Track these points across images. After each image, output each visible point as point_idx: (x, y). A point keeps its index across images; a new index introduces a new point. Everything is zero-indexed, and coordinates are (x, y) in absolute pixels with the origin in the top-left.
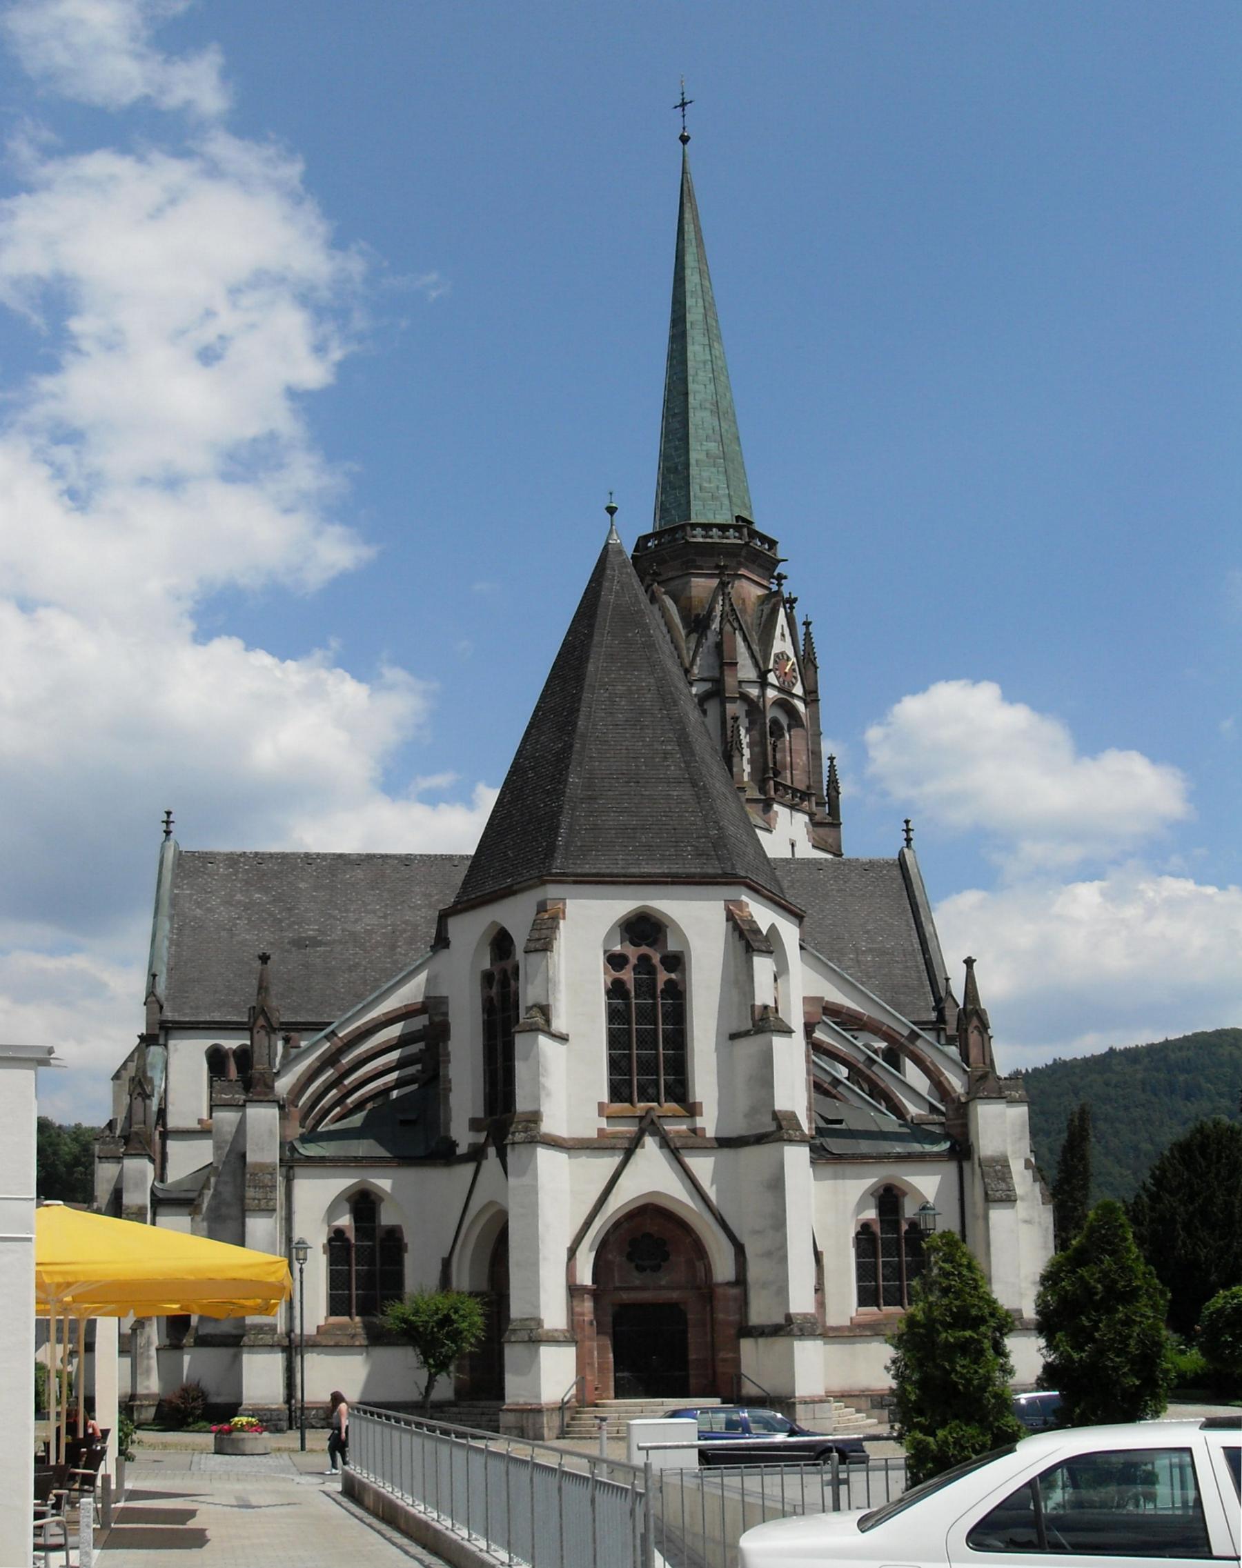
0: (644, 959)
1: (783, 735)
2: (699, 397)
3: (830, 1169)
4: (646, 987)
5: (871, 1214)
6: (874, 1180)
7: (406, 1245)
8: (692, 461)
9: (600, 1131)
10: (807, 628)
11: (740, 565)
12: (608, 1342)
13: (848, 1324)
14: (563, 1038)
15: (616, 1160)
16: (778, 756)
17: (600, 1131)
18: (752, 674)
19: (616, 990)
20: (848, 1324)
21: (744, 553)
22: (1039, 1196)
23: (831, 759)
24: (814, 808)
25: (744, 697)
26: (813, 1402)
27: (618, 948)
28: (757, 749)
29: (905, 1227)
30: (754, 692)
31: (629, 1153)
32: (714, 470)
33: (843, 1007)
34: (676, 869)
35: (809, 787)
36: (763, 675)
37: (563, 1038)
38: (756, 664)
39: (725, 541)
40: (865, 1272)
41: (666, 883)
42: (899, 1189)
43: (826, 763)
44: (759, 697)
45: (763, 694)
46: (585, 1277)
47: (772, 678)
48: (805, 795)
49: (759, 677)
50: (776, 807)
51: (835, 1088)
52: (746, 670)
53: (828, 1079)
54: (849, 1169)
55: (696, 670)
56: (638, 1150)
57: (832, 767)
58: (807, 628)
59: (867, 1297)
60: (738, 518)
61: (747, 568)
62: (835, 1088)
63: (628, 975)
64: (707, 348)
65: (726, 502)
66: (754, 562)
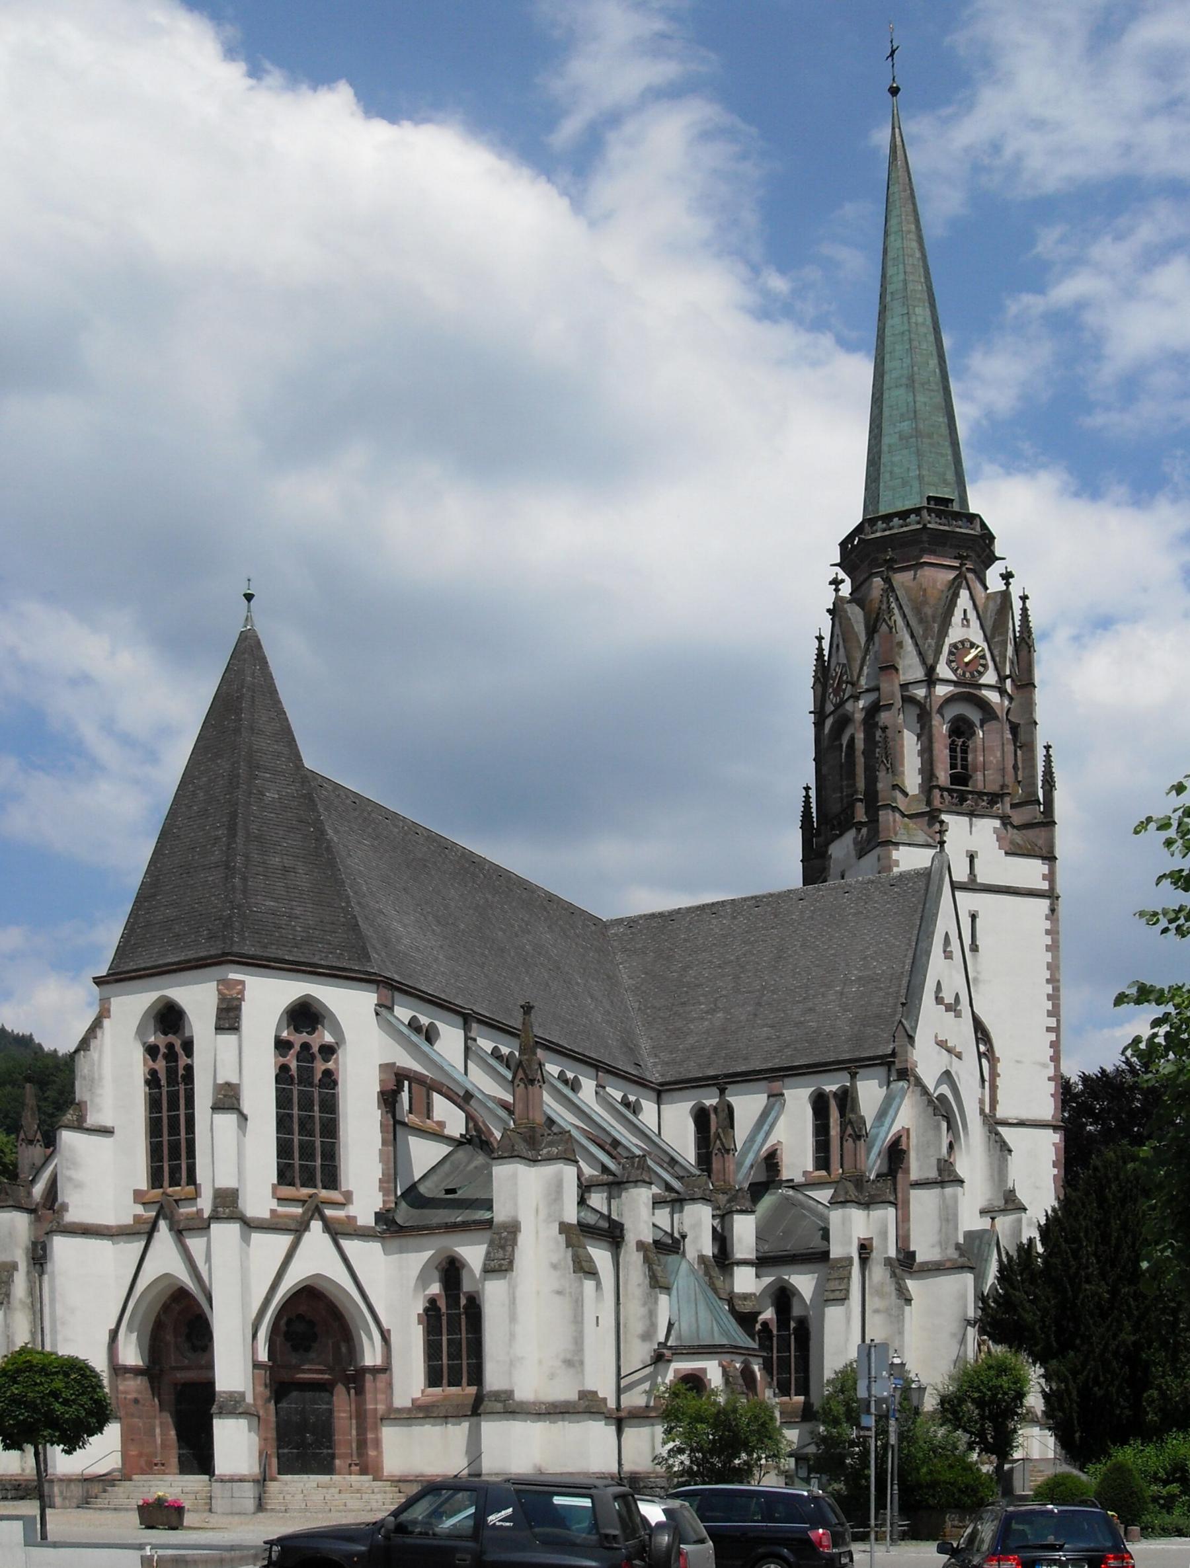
0: (170, 1046)
1: (974, 733)
2: (895, 374)
3: (395, 1243)
4: (171, 1072)
5: (435, 1288)
6: (431, 1252)
7: (420, 1323)
8: (885, 448)
9: (273, 1211)
10: (1024, 603)
11: (924, 551)
12: (168, 1419)
13: (409, 1405)
14: (107, 1132)
15: (143, 1243)
16: (970, 758)
17: (273, 1211)
18: (919, 673)
19: (152, 1081)
20: (409, 1405)
21: (925, 538)
22: (571, 1263)
23: (1048, 748)
24: (1008, 810)
25: (909, 700)
26: (241, 1481)
27: (152, 1039)
28: (926, 756)
29: (463, 1301)
30: (920, 692)
31: (150, 1235)
32: (905, 452)
33: (410, 1070)
34: (191, 954)
35: (1003, 787)
36: (930, 671)
37: (107, 1132)
38: (923, 661)
39: (905, 529)
40: (432, 1351)
41: (175, 971)
42: (460, 1261)
43: (1040, 753)
44: (926, 697)
45: (929, 695)
46: (263, 1356)
47: (943, 671)
48: (995, 798)
49: (926, 675)
50: (944, 817)
51: (615, 1148)
52: (911, 668)
53: (609, 1141)
54: (411, 1241)
55: (863, 681)
56: (156, 1234)
57: (1048, 757)
58: (1024, 603)
59: (434, 1378)
60: (929, 498)
61: (933, 552)
62: (615, 1148)
63: (161, 1065)
64: (905, 318)
65: (916, 484)
66: (944, 545)
